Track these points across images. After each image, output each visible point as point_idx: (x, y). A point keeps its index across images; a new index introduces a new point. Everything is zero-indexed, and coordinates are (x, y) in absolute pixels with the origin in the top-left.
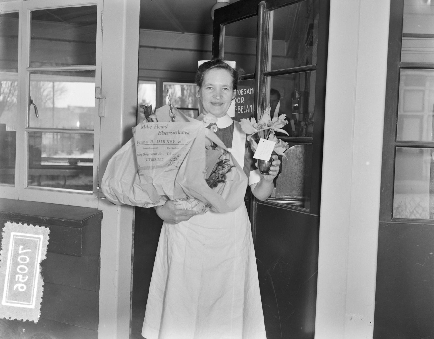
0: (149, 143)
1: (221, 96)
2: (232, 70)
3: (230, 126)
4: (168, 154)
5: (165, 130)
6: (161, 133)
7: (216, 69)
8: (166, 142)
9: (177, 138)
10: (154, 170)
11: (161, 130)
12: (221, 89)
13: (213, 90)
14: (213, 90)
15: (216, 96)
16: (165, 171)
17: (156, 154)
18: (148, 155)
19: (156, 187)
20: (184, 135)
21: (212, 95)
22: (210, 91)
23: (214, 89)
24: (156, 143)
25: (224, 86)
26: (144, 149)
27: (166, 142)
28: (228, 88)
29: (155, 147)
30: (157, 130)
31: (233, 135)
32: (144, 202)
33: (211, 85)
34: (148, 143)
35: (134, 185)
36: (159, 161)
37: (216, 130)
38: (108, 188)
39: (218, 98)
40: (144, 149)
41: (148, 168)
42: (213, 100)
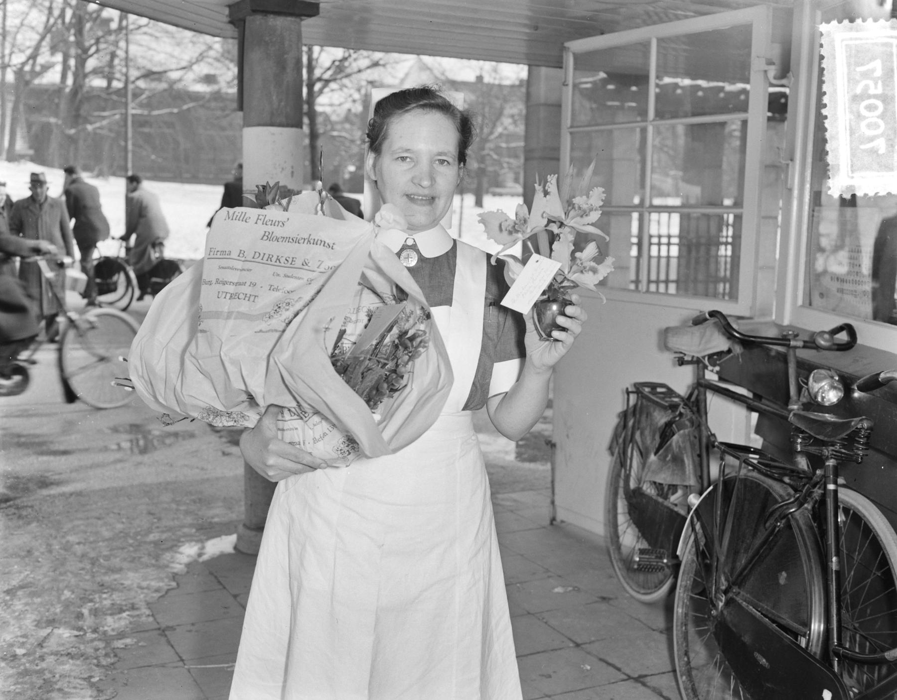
0: (234, 255)
1: (432, 179)
2: (459, 115)
3: (447, 253)
4: (272, 288)
5: (278, 231)
6: (268, 237)
7: (419, 111)
8: (274, 259)
9: (302, 252)
10: (231, 322)
11: (270, 228)
12: (432, 162)
13: (413, 164)
14: (413, 164)
15: (421, 180)
16: (258, 329)
17: (244, 284)
18: (224, 283)
19: (227, 364)
20: (319, 249)
21: (409, 176)
22: (405, 166)
23: (415, 162)
24: (250, 258)
25: (440, 154)
26: (220, 268)
27: (274, 259)
28: (450, 160)
29: (245, 268)
30: (261, 229)
31: (454, 275)
32: (204, 405)
33: (407, 150)
34: (232, 256)
35: (187, 355)
36: (246, 302)
37: (413, 262)
38: (138, 364)
39: (426, 183)
40: (220, 268)
41: (217, 315)
42: (412, 189)
